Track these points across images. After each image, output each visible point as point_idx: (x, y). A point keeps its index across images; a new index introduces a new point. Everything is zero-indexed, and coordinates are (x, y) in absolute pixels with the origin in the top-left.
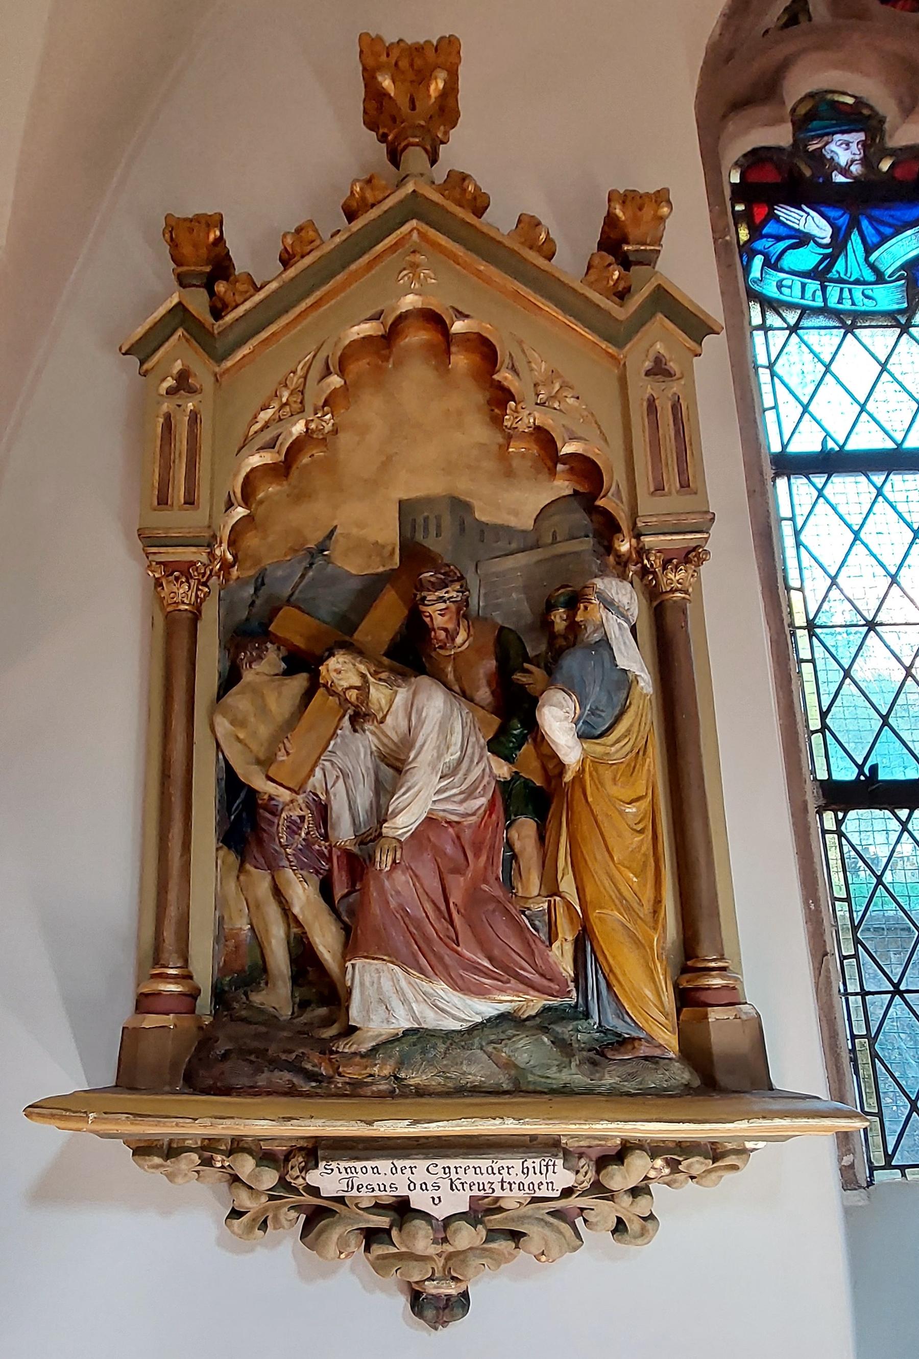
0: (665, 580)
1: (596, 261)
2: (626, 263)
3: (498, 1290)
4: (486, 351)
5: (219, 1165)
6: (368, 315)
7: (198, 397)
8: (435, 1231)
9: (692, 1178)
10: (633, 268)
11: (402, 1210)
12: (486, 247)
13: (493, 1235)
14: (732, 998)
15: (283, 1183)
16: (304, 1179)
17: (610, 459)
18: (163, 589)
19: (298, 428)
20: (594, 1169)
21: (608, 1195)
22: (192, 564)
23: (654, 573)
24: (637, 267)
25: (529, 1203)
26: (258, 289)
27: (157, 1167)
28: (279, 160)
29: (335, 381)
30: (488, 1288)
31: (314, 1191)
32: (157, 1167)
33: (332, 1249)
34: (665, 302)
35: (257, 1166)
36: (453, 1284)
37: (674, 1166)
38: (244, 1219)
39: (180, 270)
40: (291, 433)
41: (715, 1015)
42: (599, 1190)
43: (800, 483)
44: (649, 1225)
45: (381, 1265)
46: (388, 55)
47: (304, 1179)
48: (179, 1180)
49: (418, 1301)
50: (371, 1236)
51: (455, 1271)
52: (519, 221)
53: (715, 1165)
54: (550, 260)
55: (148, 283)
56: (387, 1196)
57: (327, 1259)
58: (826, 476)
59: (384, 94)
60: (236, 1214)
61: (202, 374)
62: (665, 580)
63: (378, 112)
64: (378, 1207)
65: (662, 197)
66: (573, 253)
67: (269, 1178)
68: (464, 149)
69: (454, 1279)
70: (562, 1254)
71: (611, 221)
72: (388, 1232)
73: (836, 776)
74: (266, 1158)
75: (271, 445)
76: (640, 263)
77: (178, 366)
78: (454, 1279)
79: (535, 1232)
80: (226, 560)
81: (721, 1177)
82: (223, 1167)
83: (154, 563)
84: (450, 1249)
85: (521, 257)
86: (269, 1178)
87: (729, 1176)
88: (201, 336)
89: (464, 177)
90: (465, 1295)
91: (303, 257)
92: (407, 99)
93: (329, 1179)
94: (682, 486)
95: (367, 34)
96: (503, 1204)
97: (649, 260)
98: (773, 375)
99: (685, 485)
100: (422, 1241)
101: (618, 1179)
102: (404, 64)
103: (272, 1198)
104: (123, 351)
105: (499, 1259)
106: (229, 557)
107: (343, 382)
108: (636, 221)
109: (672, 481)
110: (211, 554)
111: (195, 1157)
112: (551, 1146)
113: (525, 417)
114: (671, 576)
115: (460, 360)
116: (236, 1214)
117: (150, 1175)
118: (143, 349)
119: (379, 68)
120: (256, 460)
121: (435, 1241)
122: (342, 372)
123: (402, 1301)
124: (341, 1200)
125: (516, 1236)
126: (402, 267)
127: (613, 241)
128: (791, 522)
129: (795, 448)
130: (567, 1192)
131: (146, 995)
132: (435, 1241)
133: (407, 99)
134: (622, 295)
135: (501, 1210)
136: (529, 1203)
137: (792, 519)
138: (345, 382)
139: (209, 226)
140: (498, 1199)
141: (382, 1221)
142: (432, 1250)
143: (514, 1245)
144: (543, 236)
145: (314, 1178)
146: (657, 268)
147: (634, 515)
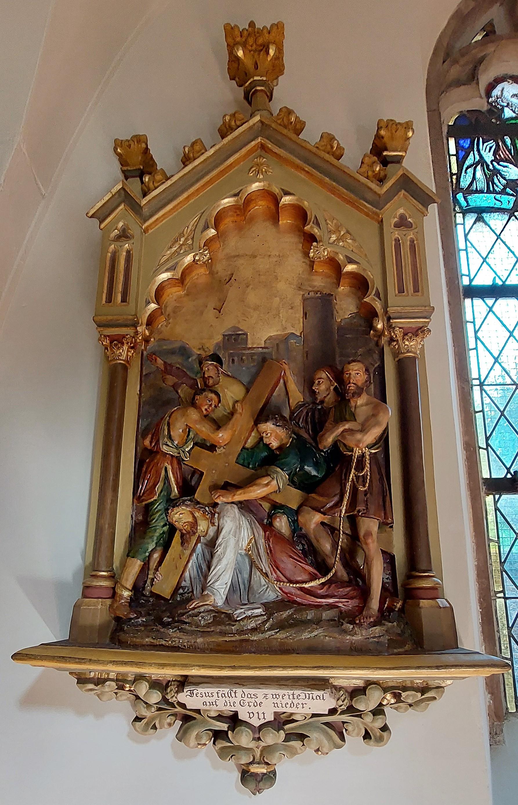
0: (403, 345)
1: (367, 160)
2: (385, 162)
3: (294, 769)
4: (301, 215)
5: (127, 689)
6: (232, 192)
7: (131, 241)
8: (254, 733)
9: (410, 705)
10: (389, 166)
11: (234, 720)
12: (303, 146)
13: (289, 737)
14: (435, 592)
15: (165, 700)
16: (176, 698)
17: (373, 275)
18: (108, 351)
19: (189, 259)
20: (349, 699)
21: (359, 714)
22: (124, 337)
23: (397, 341)
24: (391, 165)
25: (311, 718)
26: (168, 179)
27: (91, 690)
28: (180, 100)
29: (212, 232)
30: (285, 767)
31: (183, 706)
32: (91, 690)
33: (193, 741)
34: (408, 183)
35: (150, 688)
36: (266, 767)
37: (397, 697)
38: (144, 721)
39: (125, 168)
40: (184, 263)
41: (424, 603)
42: (351, 710)
43: (478, 302)
44: (385, 734)
45: (223, 753)
46: (241, 36)
47: (176, 698)
48: (105, 698)
49: (246, 776)
50: (218, 735)
51: (267, 759)
52: (322, 137)
53: (423, 697)
54: (339, 160)
55: (103, 176)
56: (228, 710)
57: (188, 746)
58: (495, 299)
59: (238, 58)
60: (138, 719)
61: (135, 230)
62: (403, 345)
63: (237, 72)
64: (220, 718)
65: (408, 126)
66: (354, 155)
67: (155, 697)
68: (287, 93)
69: (267, 764)
70: (330, 750)
71: (378, 137)
72: (226, 732)
73: (493, 477)
74: (155, 685)
75: (172, 269)
76: (392, 162)
77: (121, 224)
78: (267, 764)
79: (315, 736)
80: (145, 334)
81: (428, 704)
82: (130, 690)
83: (103, 336)
84: (262, 744)
85: (322, 162)
86: (155, 697)
87: (432, 703)
88: (135, 207)
89: (290, 112)
90: (274, 773)
91: (195, 159)
92: (252, 61)
93: (192, 699)
94: (414, 292)
95: (229, 24)
96: (294, 717)
97: (398, 160)
98: (482, 390)
99: (416, 290)
100: (244, 739)
101: (365, 705)
102: (251, 41)
103: (160, 709)
104: (90, 214)
105: (293, 753)
106: (147, 333)
107: (216, 233)
108: (392, 138)
109: (410, 286)
110: (137, 333)
111: (113, 684)
112: (320, 684)
113: (321, 252)
114: (407, 343)
115: (285, 221)
116: (138, 719)
117: (87, 695)
118: (101, 216)
119: (236, 44)
120: (164, 276)
121: (254, 739)
122: (216, 227)
123: (237, 775)
124: (198, 711)
125: (302, 737)
126: (251, 166)
127: (378, 149)
128: (463, 226)
129: (477, 282)
130: (333, 712)
131: (88, 587)
132: (254, 739)
133: (252, 61)
134: (381, 180)
135: (294, 721)
136: (311, 718)
137: (469, 276)
138: (218, 233)
139: (139, 141)
140: (292, 714)
141: (223, 726)
142: (252, 745)
143: (302, 744)
144: (335, 146)
145: (183, 697)
146: (403, 165)
147: (386, 306)
